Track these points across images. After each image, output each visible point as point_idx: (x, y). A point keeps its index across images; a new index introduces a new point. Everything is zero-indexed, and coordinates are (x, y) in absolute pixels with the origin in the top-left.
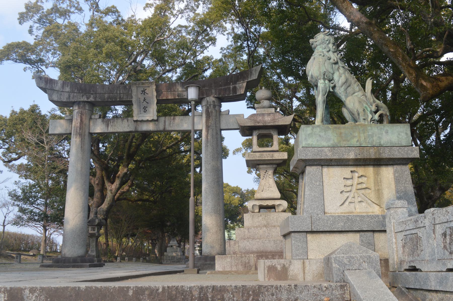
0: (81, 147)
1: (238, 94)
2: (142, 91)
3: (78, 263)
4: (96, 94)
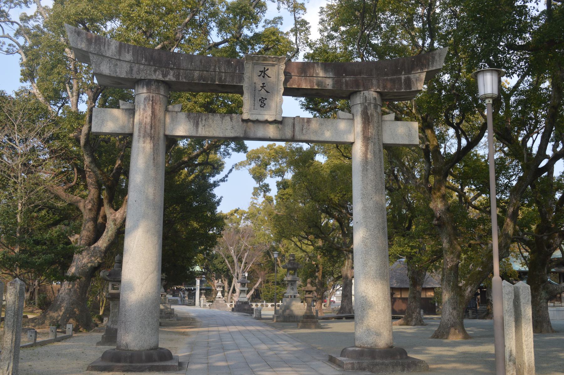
0: (154, 158)
1: (413, 89)
2: (262, 72)
3: (155, 361)
4: (178, 69)
